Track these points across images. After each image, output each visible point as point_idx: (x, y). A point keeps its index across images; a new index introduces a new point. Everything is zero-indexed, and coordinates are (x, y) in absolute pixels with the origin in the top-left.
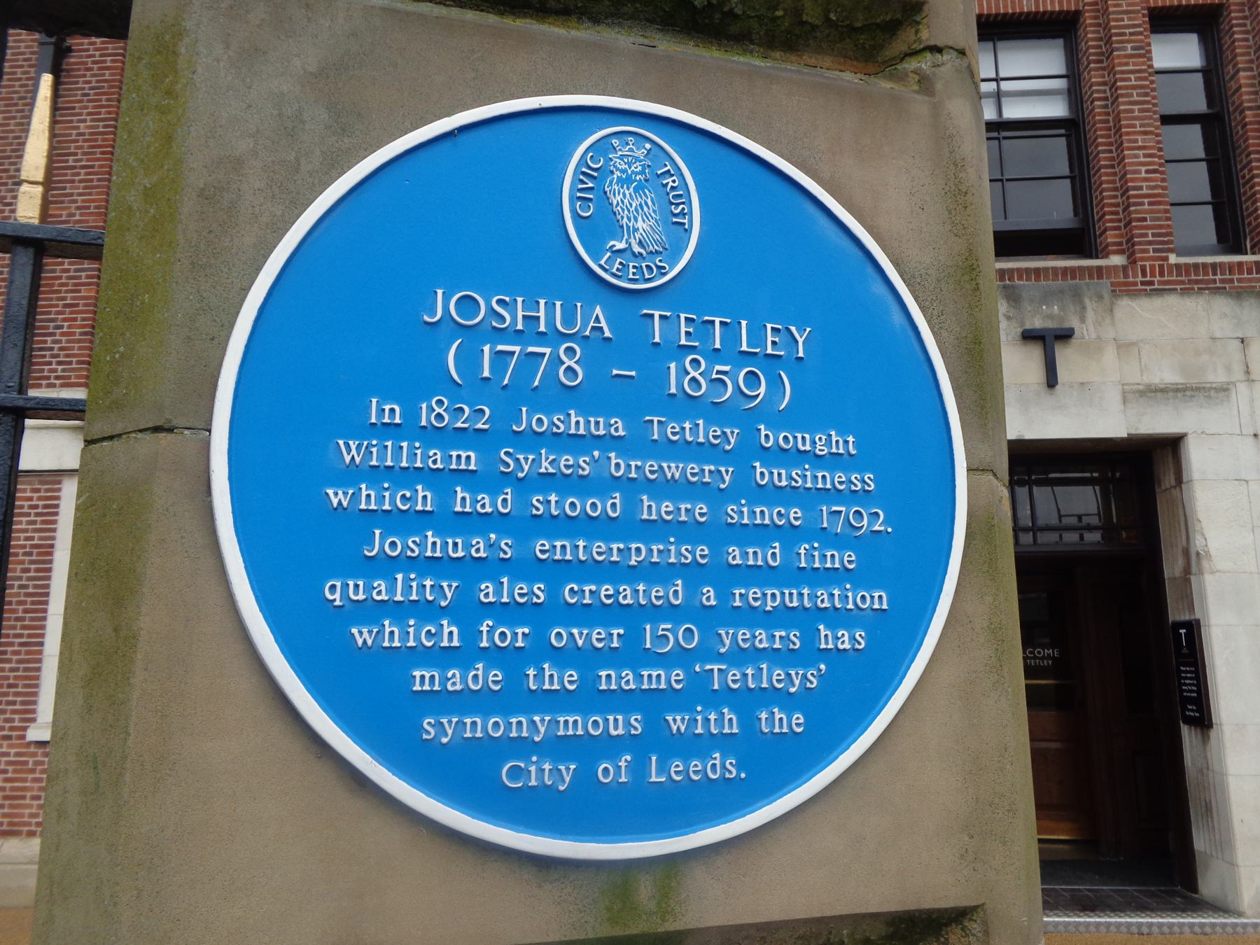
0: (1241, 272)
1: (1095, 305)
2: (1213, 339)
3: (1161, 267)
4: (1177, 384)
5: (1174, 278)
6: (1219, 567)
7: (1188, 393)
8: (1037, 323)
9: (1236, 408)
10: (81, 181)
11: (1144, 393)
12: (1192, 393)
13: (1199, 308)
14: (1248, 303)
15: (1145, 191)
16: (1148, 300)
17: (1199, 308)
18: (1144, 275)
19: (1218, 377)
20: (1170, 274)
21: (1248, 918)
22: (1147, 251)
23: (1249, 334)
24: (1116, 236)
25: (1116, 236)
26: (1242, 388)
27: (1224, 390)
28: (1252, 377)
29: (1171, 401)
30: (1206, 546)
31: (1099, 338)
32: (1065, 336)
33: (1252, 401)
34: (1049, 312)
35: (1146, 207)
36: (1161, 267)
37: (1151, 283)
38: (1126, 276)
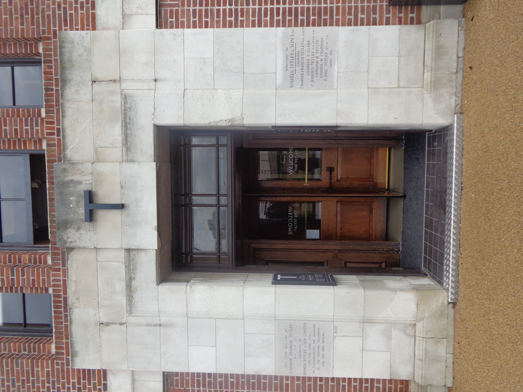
0: (51, 73)
1: (69, 174)
2: (92, 100)
3: (47, 123)
4: (122, 127)
5: (55, 115)
6: (240, 115)
7: (128, 121)
8: (82, 211)
9: (138, 91)
11: (127, 148)
12: (128, 118)
13: (72, 106)
14: (69, 75)
16: (67, 138)
17: (72, 106)
18: (53, 134)
19: (117, 99)
20: (52, 117)
21: (454, 121)
22: (37, 131)
23: (89, 77)
24: (30, 144)
25: (30, 144)
26: (124, 85)
27: (125, 98)
28: (117, 78)
29: (133, 132)
30: (226, 121)
31: (91, 174)
32: (90, 196)
33: (133, 80)
34: (75, 203)
35: (7, 128)
36: (47, 123)
38: (54, 145)
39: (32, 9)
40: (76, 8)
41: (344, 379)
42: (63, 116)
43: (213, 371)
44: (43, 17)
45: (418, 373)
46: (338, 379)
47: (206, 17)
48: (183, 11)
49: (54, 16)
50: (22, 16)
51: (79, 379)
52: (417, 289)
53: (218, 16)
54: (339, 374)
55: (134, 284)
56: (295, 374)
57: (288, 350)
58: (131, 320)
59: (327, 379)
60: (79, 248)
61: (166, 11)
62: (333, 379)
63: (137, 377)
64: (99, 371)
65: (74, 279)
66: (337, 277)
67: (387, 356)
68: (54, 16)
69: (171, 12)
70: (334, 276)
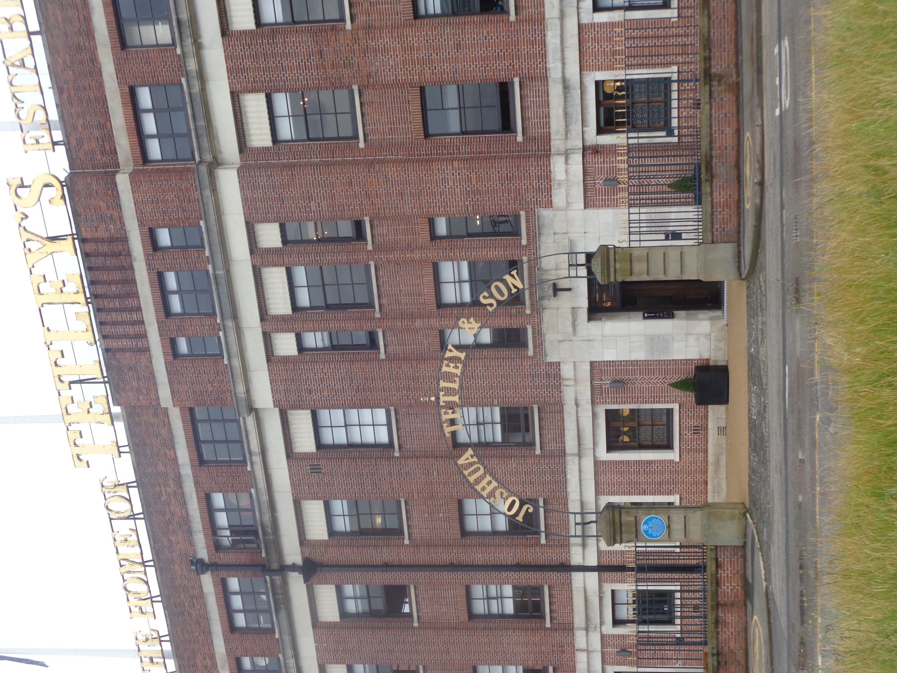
2: (554, 242)
10: (499, 555)
15: (502, 253)
19: (567, 242)
26: (570, 235)
32: (555, 285)
37: (534, 253)
39: (520, 198)
40: (542, 198)
41: (678, 360)
42: (539, 249)
43: (614, 359)
44: (525, 202)
45: (712, 355)
46: (676, 360)
47: (608, 201)
48: (596, 199)
49: (531, 201)
50: (514, 201)
51: (546, 367)
52: (711, 319)
53: (614, 201)
54: (675, 358)
55: (576, 323)
56: (655, 359)
57: (651, 349)
58: (575, 339)
59: (670, 360)
60: (549, 308)
61: (588, 200)
62: (673, 360)
63: (577, 364)
64: (556, 362)
65: (546, 321)
66: (675, 312)
67: (698, 349)
68: (531, 201)
69: (591, 199)
70: (674, 312)
